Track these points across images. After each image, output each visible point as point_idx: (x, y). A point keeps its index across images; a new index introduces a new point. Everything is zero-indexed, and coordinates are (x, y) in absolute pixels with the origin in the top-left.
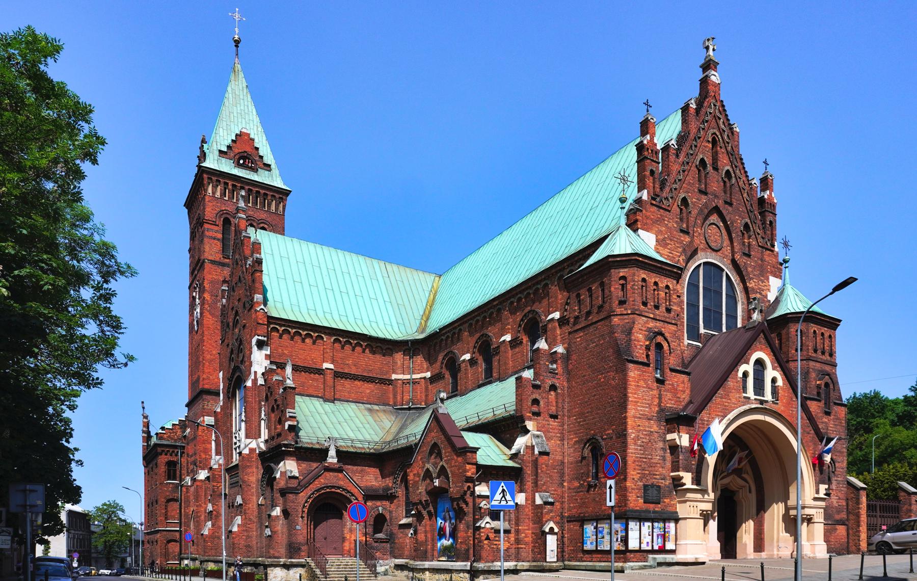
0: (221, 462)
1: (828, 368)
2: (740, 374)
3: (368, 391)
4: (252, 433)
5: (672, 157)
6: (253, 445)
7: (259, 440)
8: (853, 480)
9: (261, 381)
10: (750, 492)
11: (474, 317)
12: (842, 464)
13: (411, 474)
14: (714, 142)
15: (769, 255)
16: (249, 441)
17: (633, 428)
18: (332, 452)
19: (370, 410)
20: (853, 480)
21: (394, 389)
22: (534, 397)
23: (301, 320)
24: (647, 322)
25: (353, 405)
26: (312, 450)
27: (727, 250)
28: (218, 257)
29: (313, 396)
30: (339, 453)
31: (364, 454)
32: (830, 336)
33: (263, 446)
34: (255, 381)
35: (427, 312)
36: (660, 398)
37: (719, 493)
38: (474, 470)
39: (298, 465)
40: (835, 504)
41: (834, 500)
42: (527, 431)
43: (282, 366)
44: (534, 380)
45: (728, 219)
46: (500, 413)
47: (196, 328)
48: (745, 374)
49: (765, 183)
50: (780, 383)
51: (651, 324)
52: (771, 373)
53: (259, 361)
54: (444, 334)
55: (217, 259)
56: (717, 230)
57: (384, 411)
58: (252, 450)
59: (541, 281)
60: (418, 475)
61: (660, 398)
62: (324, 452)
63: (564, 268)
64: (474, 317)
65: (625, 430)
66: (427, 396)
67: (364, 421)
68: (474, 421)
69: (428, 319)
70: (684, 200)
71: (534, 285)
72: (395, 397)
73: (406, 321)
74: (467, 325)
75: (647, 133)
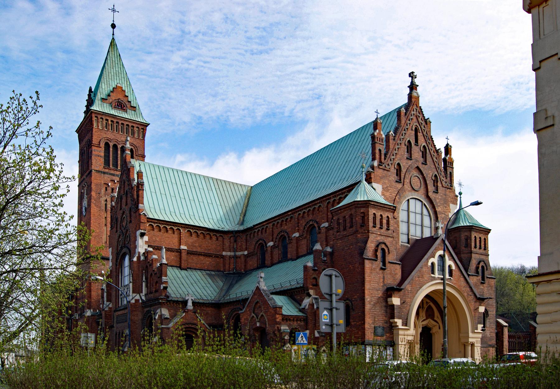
0: (111, 306)
1: (483, 257)
2: (430, 264)
3: (208, 263)
4: (137, 290)
5: (391, 141)
6: (138, 297)
7: (141, 294)
8: (501, 321)
9: (142, 258)
10: (440, 328)
11: (276, 220)
12: (492, 312)
13: (243, 319)
14: (416, 131)
15: (450, 192)
16: (134, 295)
17: (368, 295)
18: (190, 304)
19: (209, 275)
20: (501, 321)
21: (224, 261)
22: (314, 276)
23: (167, 219)
24: (376, 237)
25: (199, 272)
26: (177, 302)
27: (422, 190)
28: (101, 168)
29: (174, 266)
30: (194, 303)
31: (209, 303)
32: (485, 239)
33: (143, 298)
34: (139, 258)
35: (244, 211)
36: (384, 278)
37: (420, 330)
38: (281, 318)
39: (169, 311)
40: (488, 336)
41: (488, 333)
42: (309, 295)
43: (158, 249)
44: (314, 266)
45: (424, 173)
46: (294, 285)
47: (84, 214)
48: (433, 264)
49: (448, 149)
50: (454, 267)
51: (379, 238)
52: (449, 262)
53: (142, 246)
54: (256, 229)
55: (101, 170)
56: (418, 179)
57: (218, 275)
58: (137, 301)
59: (317, 203)
60: (247, 319)
61: (384, 278)
62: (185, 303)
63: (331, 198)
64: (276, 220)
65: (364, 296)
66: (245, 266)
67: (207, 282)
68: (278, 288)
69: (245, 215)
70: (399, 164)
71: (313, 205)
72: (224, 266)
73: (231, 218)
74: (271, 224)
75: (377, 129)
